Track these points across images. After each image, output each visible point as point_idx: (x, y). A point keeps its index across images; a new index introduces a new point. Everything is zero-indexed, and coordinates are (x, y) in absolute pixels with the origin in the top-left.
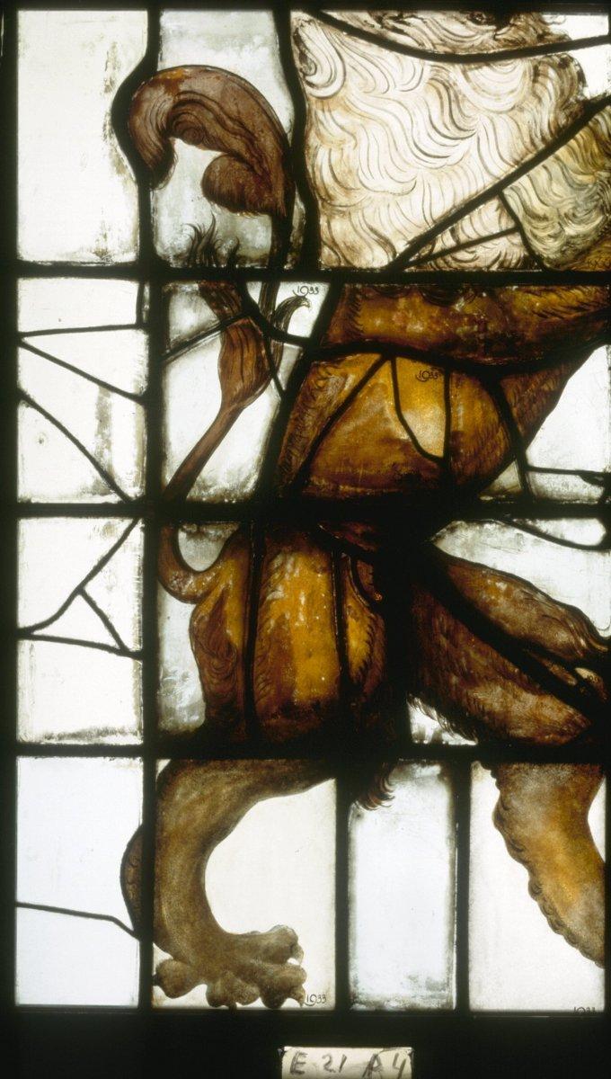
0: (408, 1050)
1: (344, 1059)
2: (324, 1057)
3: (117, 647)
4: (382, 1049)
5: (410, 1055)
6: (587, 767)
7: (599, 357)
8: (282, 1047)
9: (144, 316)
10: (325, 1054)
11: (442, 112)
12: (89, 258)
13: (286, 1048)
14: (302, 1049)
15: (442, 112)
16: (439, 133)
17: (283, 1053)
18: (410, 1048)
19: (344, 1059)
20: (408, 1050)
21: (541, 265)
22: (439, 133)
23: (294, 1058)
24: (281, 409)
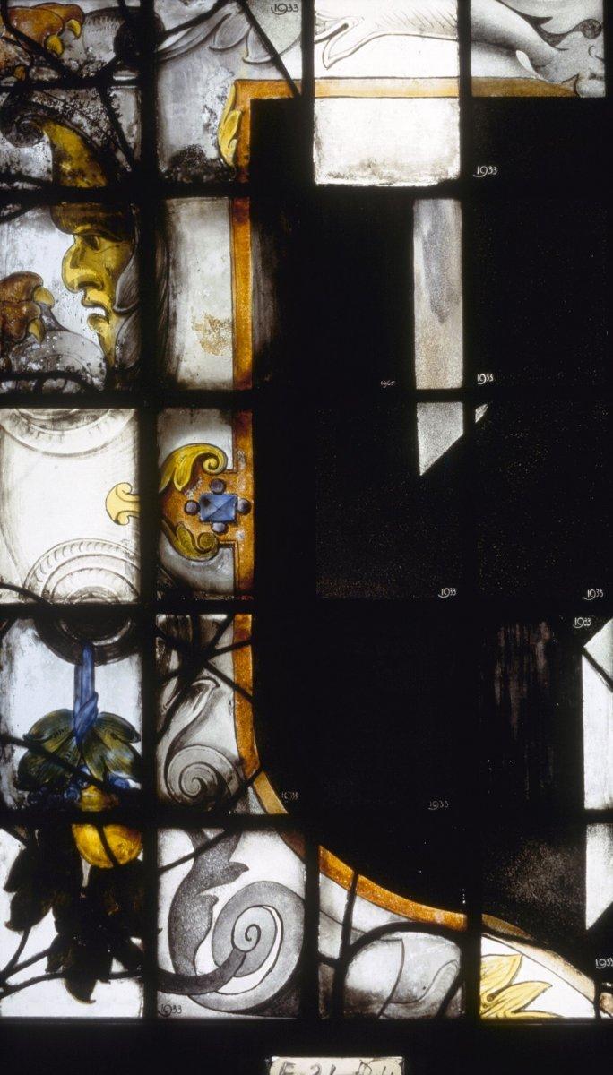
0: (399, 1059)
1: (334, 1069)
2: (312, 1068)
3: (219, 647)
4: (372, 1059)
5: (401, 1065)
6: (134, 291)
7: (609, 623)
8: (270, 1057)
9: (527, 938)
10: (313, 1064)
11: (233, 1012)
12: (426, 39)
13: (274, 1059)
14: (289, 1060)
15: (233, 1012)
16: (274, 965)
17: (271, 1063)
18: (401, 1058)
19: (334, 1069)
20: (399, 1059)
21: (586, 609)
22: (274, 965)
23: (282, 1069)
24: (398, 1020)
